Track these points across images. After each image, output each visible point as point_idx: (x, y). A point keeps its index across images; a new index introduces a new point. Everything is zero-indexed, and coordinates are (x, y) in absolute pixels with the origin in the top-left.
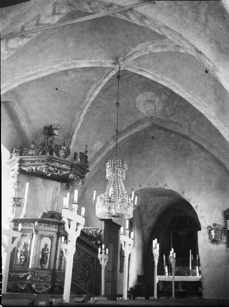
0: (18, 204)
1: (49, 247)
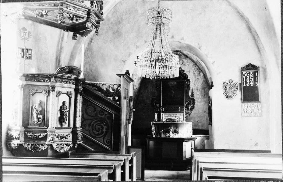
0: (28, 55)
1: (67, 104)
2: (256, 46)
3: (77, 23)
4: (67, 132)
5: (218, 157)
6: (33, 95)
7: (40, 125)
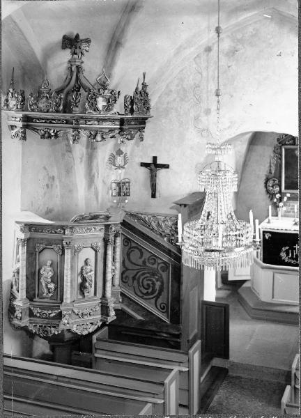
6: (40, 252)
7: (51, 298)
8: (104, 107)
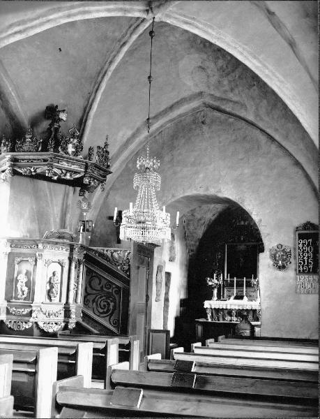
2: (208, 416)
3: (72, 179)
4: (58, 308)
5: (78, 277)
7: (25, 299)
8: (73, 152)
